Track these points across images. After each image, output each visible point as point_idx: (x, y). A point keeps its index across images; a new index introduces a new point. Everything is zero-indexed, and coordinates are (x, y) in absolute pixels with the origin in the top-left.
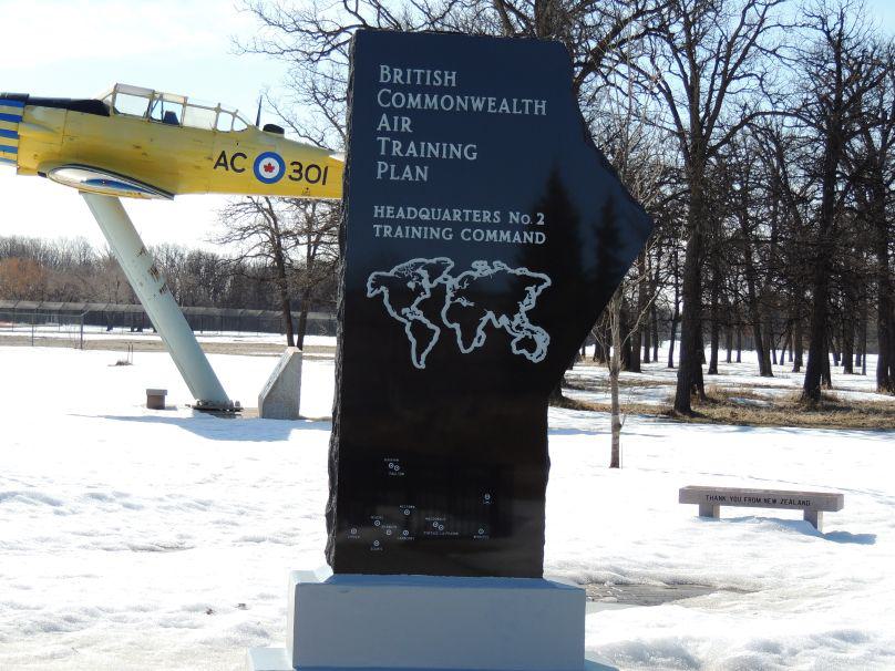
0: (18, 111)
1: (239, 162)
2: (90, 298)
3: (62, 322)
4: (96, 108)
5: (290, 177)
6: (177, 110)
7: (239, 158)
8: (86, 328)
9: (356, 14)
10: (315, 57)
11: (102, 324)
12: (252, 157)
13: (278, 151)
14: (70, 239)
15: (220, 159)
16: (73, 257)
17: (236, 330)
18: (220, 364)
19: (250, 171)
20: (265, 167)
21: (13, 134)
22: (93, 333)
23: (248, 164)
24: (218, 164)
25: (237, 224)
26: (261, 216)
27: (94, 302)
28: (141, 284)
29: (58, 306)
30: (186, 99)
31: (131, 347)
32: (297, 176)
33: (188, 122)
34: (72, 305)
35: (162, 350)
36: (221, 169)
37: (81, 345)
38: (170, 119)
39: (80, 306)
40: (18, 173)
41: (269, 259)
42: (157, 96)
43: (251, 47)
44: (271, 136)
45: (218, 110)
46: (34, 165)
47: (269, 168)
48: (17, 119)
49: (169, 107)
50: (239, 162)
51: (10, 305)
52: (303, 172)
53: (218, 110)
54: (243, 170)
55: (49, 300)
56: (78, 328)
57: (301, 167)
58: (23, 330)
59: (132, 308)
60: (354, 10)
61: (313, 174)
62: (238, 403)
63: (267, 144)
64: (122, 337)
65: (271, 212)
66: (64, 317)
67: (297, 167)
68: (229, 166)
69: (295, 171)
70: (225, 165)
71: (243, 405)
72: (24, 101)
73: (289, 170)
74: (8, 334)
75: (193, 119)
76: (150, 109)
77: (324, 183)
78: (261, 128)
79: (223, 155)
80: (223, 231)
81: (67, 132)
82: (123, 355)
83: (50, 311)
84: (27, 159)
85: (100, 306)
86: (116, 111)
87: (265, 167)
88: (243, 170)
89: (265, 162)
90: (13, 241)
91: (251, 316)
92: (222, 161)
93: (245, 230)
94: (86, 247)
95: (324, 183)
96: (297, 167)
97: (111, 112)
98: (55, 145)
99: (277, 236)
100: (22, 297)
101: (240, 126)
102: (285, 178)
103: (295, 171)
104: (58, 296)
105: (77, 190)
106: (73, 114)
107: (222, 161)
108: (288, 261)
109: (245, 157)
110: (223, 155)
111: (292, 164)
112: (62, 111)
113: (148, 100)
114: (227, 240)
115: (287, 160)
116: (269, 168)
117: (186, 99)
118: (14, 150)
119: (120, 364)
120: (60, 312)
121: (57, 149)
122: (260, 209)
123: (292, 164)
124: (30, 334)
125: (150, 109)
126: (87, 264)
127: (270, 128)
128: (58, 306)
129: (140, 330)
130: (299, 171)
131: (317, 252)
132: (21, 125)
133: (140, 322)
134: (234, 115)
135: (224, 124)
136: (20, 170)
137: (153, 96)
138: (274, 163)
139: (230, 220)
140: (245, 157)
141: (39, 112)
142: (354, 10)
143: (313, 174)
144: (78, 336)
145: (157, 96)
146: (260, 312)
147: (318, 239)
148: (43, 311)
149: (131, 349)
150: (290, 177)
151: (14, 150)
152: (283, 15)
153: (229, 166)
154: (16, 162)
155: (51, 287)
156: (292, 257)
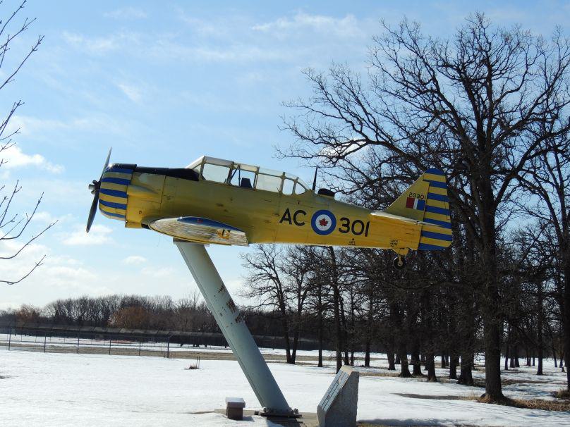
0: (128, 176)
1: (300, 218)
2: (172, 328)
3: (106, 338)
4: (189, 175)
5: (340, 230)
6: (251, 177)
7: (300, 215)
8: (171, 345)
9: (361, 132)
10: (334, 160)
11: (178, 343)
12: (310, 215)
13: (331, 210)
14: (162, 297)
15: (285, 215)
16: (163, 307)
17: (33, 335)
18: (281, 373)
19: (308, 225)
20: (324, 220)
21: (124, 195)
22: (174, 348)
23: (306, 219)
24: (284, 218)
25: (258, 286)
26: (271, 281)
27: (174, 330)
28: (221, 315)
29: (155, 332)
30: (258, 168)
31: (198, 357)
32: (345, 229)
33: (260, 186)
34: (162, 332)
35: (234, 359)
36: (286, 223)
37: (168, 355)
38: (245, 183)
39: (167, 332)
40: (126, 226)
41: (276, 306)
42: (236, 166)
43: (289, 153)
44: (324, 198)
45: (283, 177)
46: (139, 219)
47: (323, 223)
48: (127, 183)
49: (244, 175)
50: (300, 218)
51: (129, 332)
52: (350, 226)
53: (283, 177)
54: (303, 224)
55: (150, 329)
56: (166, 344)
57: (349, 223)
58: (135, 345)
59: (217, 335)
60: (359, 130)
61: (358, 228)
62: (296, 411)
63: (321, 204)
64: (189, 350)
65: (277, 279)
66: (157, 339)
67: (345, 222)
68: (292, 221)
69: (344, 225)
70: (289, 220)
71: (300, 411)
72: (133, 169)
73: (339, 225)
74: (128, 347)
75: (266, 184)
76: (230, 177)
77: (366, 235)
78: (316, 192)
79: (288, 211)
80: (248, 289)
81: (165, 193)
82: (193, 362)
83: (151, 335)
84: (134, 216)
85: (178, 333)
86: (203, 178)
87: (324, 220)
88: (303, 224)
89: (321, 217)
90: (132, 299)
91: (308, 338)
92: (287, 217)
93: (261, 289)
94: (170, 301)
95: (366, 235)
96: (345, 222)
97: (200, 178)
98: (157, 202)
99: (280, 296)
100: (136, 328)
101: (299, 190)
102: (336, 231)
103: (344, 225)
104: (155, 328)
105: (172, 238)
106: (169, 179)
107: (287, 217)
108: (287, 308)
109: (305, 214)
110: (288, 211)
111: (342, 219)
112: (162, 177)
113: (229, 169)
114: (251, 295)
115: (338, 217)
116: (323, 223)
117: (258, 168)
118: (124, 207)
119: (192, 368)
120: (155, 335)
121: (157, 206)
122: (271, 277)
123: (342, 219)
124: (138, 347)
125: (230, 177)
126: (170, 311)
127: (323, 191)
128: (155, 332)
129: (198, 346)
130: (347, 226)
131: (304, 302)
132: (130, 188)
133: (222, 342)
134: (296, 181)
135: (287, 191)
136: (129, 224)
137: (233, 167)
138: (328, 218)
139: (254, 284)
140: (305, 214)
141: (144, 178)
142: (359, 130)
143: (358, 228)
144: (166, 349)
145: (236, 166)
146: (262, 337)
147: (305, 293)
148: (147, 335)
149: (198, 358)
150: (340, 230)
151: (124, 207)
152: (312, 130)
153: (292, 221)
154: (125, 217)
155: (151, 322)
156: (290, 305)
